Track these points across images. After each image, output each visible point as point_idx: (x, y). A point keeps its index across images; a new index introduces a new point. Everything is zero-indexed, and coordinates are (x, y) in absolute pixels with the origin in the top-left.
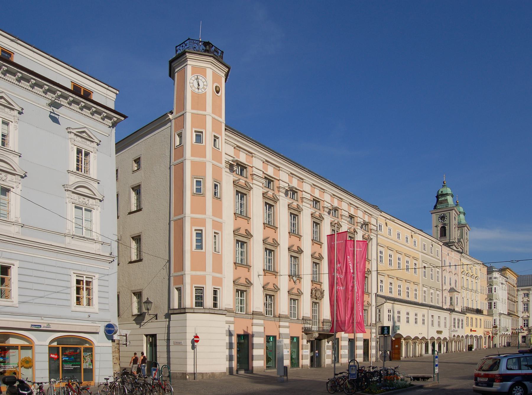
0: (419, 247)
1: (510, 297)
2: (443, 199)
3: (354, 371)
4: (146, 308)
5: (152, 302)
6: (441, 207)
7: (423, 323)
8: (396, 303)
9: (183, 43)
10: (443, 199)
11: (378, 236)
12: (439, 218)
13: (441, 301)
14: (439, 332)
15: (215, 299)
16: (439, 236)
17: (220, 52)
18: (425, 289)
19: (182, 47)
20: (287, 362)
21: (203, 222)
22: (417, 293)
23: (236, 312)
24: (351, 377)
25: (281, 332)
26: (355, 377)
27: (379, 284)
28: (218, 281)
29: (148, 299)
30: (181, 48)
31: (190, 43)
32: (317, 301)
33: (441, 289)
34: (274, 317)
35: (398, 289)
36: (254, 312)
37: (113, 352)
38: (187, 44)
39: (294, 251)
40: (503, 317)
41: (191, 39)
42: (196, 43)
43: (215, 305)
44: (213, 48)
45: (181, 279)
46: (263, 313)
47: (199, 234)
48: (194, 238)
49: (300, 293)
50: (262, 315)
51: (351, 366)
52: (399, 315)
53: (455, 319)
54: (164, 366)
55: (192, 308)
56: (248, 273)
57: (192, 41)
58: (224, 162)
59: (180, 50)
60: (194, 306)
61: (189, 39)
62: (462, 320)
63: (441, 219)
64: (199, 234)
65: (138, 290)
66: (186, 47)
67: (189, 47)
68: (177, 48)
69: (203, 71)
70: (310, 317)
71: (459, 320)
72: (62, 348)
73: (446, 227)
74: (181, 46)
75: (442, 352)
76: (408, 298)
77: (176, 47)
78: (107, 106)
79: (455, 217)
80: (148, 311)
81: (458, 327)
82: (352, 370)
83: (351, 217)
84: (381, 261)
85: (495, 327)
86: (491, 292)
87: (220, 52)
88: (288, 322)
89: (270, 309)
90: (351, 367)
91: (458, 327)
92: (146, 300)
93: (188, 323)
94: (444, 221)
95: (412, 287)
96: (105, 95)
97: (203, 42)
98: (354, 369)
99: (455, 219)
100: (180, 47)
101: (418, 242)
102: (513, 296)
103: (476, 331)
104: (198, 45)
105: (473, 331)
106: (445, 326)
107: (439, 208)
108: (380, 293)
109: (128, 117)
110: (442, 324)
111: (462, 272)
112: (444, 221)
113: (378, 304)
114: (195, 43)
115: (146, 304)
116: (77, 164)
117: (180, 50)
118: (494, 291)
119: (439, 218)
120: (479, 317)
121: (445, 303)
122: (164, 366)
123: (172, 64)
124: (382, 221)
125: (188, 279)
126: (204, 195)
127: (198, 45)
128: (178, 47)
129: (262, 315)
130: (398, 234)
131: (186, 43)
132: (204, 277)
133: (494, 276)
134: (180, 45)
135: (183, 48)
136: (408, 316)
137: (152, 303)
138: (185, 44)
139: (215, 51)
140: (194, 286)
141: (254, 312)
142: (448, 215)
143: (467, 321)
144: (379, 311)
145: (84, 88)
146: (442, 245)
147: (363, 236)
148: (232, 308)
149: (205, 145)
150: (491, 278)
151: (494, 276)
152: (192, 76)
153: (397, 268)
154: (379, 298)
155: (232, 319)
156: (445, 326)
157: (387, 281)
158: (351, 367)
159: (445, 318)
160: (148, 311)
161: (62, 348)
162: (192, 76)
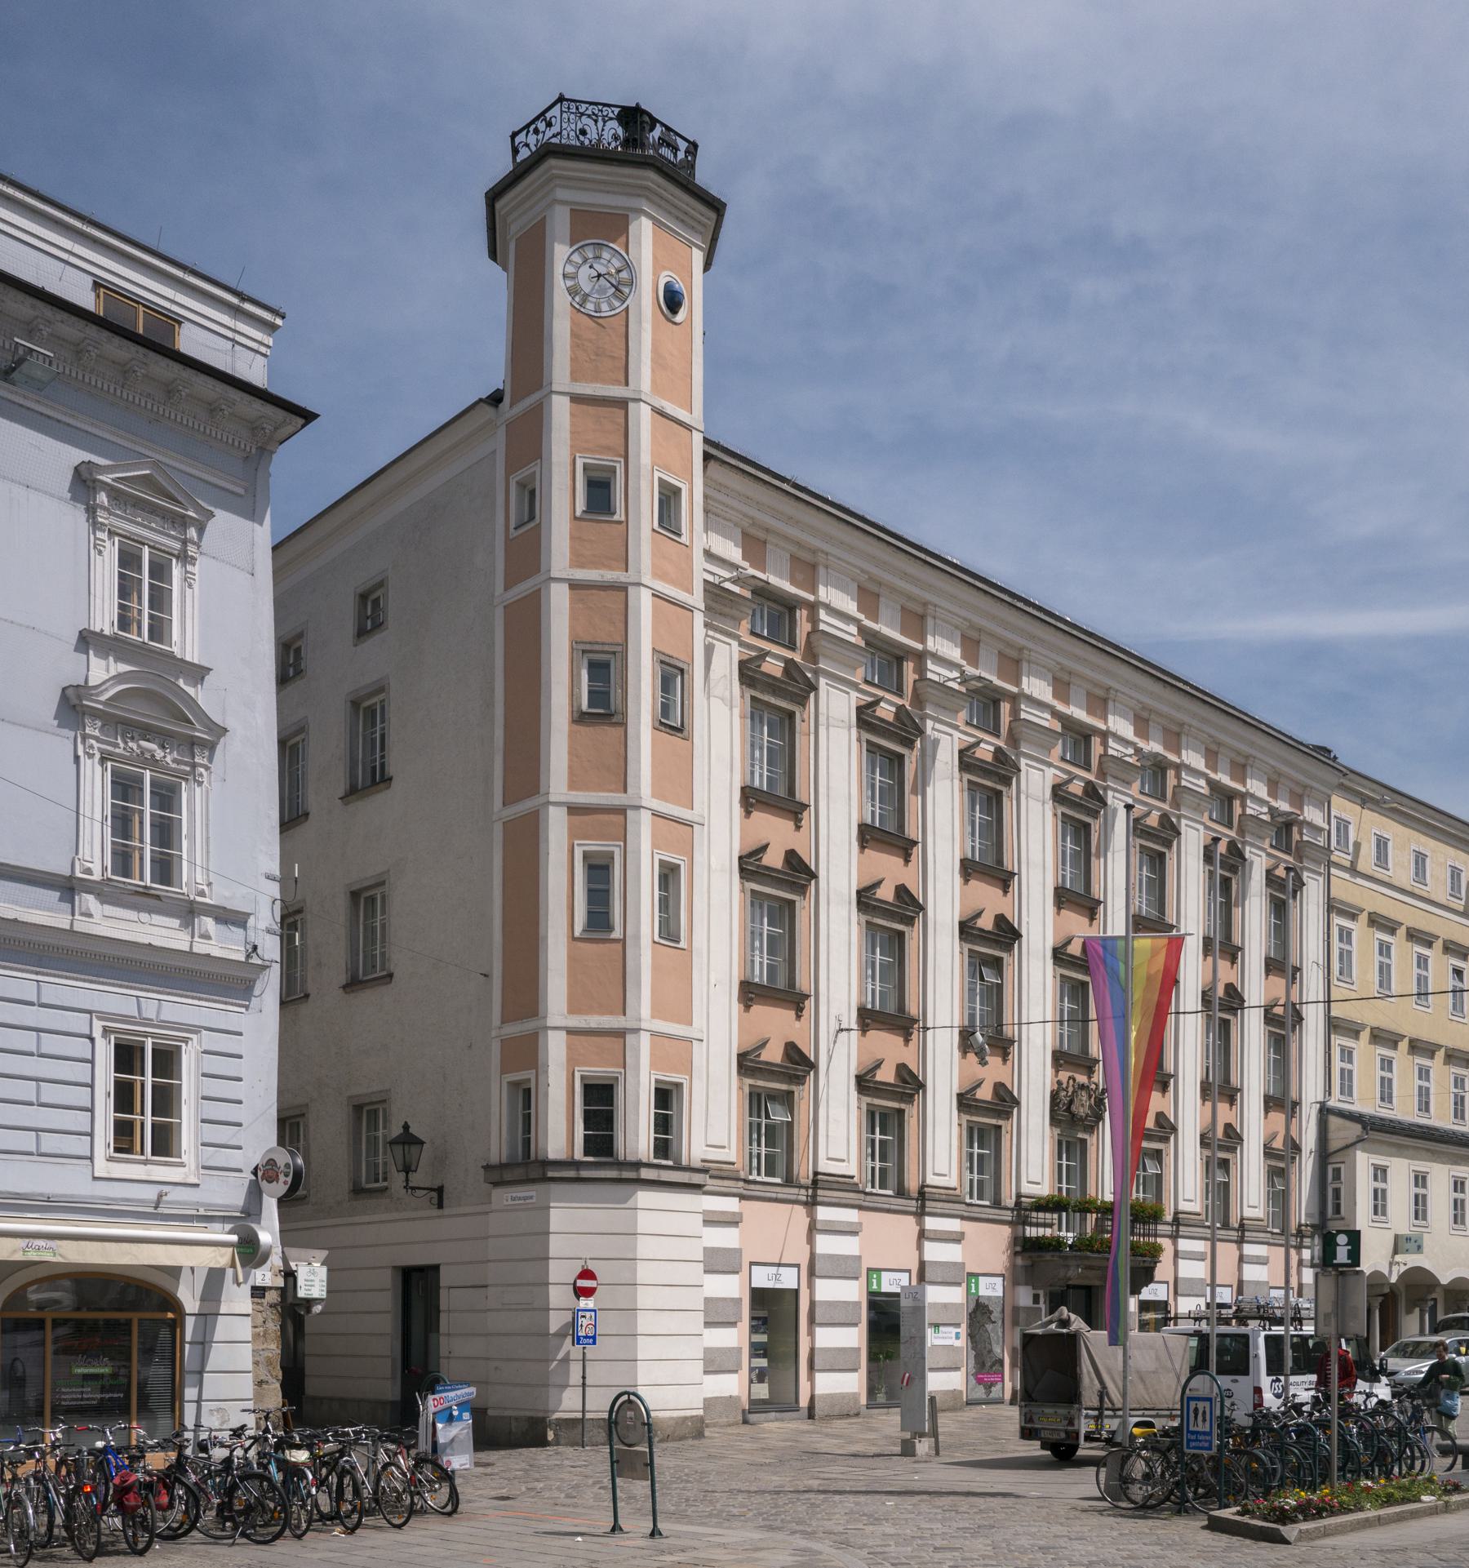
3: (1204, 1420)
4: (400, 1162)
5: (422, 1137)
9: (537, 118)
15: (663, 1124)
17: (683, 145)
19: (536, 131)
23: (751, 1178)
24: (1193, 1444)
25: (927, 1257)
26: (1206, 1445)
27: (1337, 1064)
28: (676, 1050)
29: (406, 1127)
30: (532, 139)
31: (565, 115)
35: (1419, 1083)
36: (820, 1177)
37: (256, 1336)
38: (553, 120)
41: (567, 100)
42: (589, 112)
43: (663, 1148)
44: (657, 132)
46: (856, 1180)
47: (599, 871)
49: (1005, 1102)
50: (855, 1189)
51: (1190, 1399)
54: (625, 1397)
57: (573, 105)
58: (699, 588)
59: (527, 145)
60: (579, 1154)
61: (561, 99)
64: (599, 871)
65: (373, 1093)
66: (549, 134)
67: (560, 133)
68: (517, 140)
70: (733, 1164)
72: (140, 1320)
74: (532, 128)
77: (514, 135)
78: (237, 375)
80: (407, 1173)
82: (1196, 1418)
87: (683, 145)
88: (734, 1195)
89: (755, 1152)
90: (1193, 1404)
92: (401, 1131)
96: (230, 334)
97: (617, 110)
98: (1204, 1412)
100: (528, 132)
104: (596, 121)
109: (318, 416)
114: (582, 114)
115: (398, 1149)
116: (121, 606)
117: (527, 145)
122: (625, 1397)
123: (498, 205)
125: (556, 1047)
127: (596, 121)
128: (521, 138)
131: (548, 115)
134: (528, 126)
135: (541, 136)
137: (422, 1143)
138: (545, 120)
139: (664, 141)
141: (820, 1177)
144: (1337, 1172)
145: (144, 306)
148: (733, 1159)
152: (575, 248)
153: (1374, 989)
154: (1334, 1121)
155: (731, 1205)
158: (1193, 1404)
160: (407, 1173)
161: (140, 1320)
162: (575, 248)
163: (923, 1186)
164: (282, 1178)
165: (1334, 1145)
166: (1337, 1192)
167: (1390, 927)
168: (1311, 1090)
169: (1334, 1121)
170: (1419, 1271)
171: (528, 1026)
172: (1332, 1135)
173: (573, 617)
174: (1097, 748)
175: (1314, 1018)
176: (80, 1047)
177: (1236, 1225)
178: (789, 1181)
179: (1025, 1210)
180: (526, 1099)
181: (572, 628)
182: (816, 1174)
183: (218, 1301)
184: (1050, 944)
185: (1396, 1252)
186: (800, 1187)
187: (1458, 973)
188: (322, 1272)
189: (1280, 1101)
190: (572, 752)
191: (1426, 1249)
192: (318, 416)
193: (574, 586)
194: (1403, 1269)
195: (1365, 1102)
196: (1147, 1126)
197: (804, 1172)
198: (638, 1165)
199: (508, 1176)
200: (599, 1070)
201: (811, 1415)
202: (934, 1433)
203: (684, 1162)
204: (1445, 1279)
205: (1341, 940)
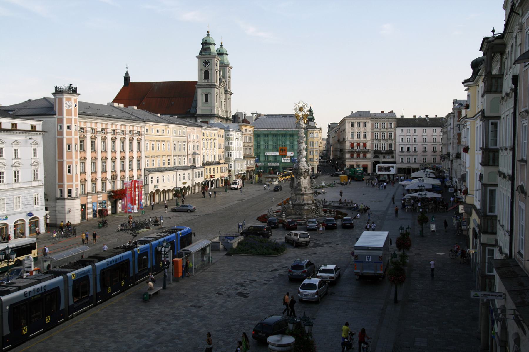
0: (171, 133)
2: (207, 46)
6: (205, 54)
10: (207, 46)
12: (204, 63)
13: (187, 162)
14: (185, 183)
16: (203, 78)
18: (175, 158)
20: (306, 281)
21: (71, 163)
22: (170, 161)
27: (146, 162)
34: (95, 193)
39: (104, 160)
40: (237, 162)
43: (61, 196)
45: (62, 186)
48: (68, 169)
50: (91, 193)
53: (196, 173)
55: (67, 198)
56: (85, 176)
63: (205, 64)
69: (70, 100)
73: (209, 71)
75: (188, 194)
79: (216, 63)
84: (147, 149)
85: (229, 171)
93: (66, 204)
94: (207, 66)
95: (166, 159)
99: (217, 64)
101: (171, 132)
106: (189, 178)
107: (203, 55)
109: (196, 56)
112: (207, 66)
113: (146, 174)
118: (230, 144)
119: (204, 63)
121: (190, 162)
125: (66, 186)
126: (71, 151)
129: (91, 193)
130: (158, 130)
132: (72, 185)
133: (230, 134)
140: (68, 189)
142: (210, 61)
144: (146, 178)
150: (228, 135)
151: (230, 134)
154: (146, 171)
156: (189, 178)
157: (150, 160)
166: (147, 181)
167: (159, 141)
168: (143, 167)
176: (12, 199)
179: (109, 192)
180: (62, 192)
184: (111, 158)
188: (431, 227)
192: (196, 56)
195: (150, 166)
196: (289, 161)
197: (86, 193)
198: (75, 198)
201: (87, 220)
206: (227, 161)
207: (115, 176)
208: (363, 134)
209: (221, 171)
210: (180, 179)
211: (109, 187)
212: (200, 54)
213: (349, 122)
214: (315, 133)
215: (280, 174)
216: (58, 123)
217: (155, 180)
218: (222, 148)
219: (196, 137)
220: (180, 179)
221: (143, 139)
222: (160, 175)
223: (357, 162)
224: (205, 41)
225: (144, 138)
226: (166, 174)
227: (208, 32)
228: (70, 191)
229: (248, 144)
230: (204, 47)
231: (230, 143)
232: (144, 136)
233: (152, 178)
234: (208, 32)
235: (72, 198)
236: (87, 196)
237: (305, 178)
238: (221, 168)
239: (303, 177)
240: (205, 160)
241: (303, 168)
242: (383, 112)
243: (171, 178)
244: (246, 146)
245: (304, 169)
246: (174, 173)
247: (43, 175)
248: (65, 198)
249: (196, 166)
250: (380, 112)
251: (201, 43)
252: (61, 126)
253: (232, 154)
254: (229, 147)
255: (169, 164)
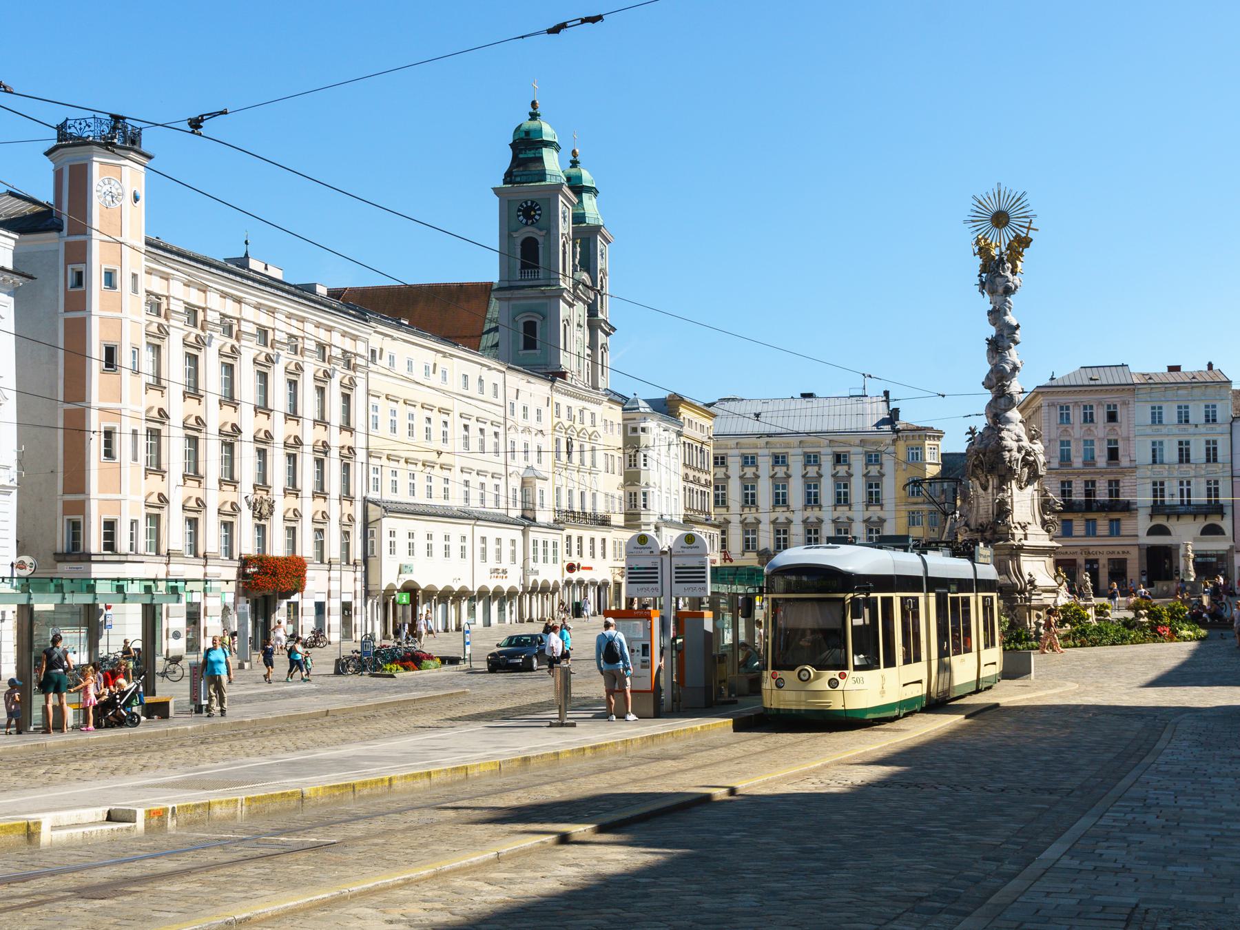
1: (691, 473)
2: (530, 154)
7: (463, 556)
8: (479, 523)
10: (530, 154)
11: (370, 374)
32: (263, 522)
33: (504, 473)
48: (103, 448)
52: (392, 539)
53: (535, 543)
62: (555, 544)
71: (545, 543)
72: (883, 598)
76: (429, 499)
81: (545, 560)
83: (322, 347)
86: (635, 465)
91: (545, 560)
95: (403, 471)
102: (700, 470)
103: (590, 568)
105: (584, 568)
106: (514, 559)
108: (373, 495)
109: (494, 189)
110: (506, 555)
111: (555, 427)
118: (642, 462)
119: (519, 210)
120: (599, 534)
124: (376, 341)
136: (447, 543)
143: (569, 545)
144: (372, 532)
146: (504, 370)
147: (184, 340)
149: (70, 267)
154: (371, 506)
156: (514, 559)
159: (513, 541)
163: (205, 553)
164: (28, 568)
165: (371, 518)
168: (358, 490)
169: (371, 506)
170: (410, 581)
171: (80, 497)
172: (370, 514)
173: (101, 331)
174: (270, 337)
175: (361, 455)
177: (165, 554)
178: (158, 554)
179: (245, 562)
180: (76, 530)
181: (100, 335)
182: (168, 550)
183: (919, 579)
185: (400, 573)
186: (163, 556)
187: (429, 419)
189: (347, 496)
190: (100, 385)
191: (414, 571)
193: (101, 317)
194: (404, 581)
199: (68, 558)
200: (110, 517)
202: (250, 661)
203: (119, 552)
204: (423, 586)
205: (373, 410)
206: (632, 519)
207: (266, 506)
208: (1105, 446)
209: (615, 556)
210: (484, 557)
211: (247, 545)
212: (505, 182)
213: (1053, 405)
214: (927, 447)
215: (915, 486)
216: (68, 262)
217: (402, 542)
218: (616, 471)
219: (532, 414)
220: (484, 557)
221: (361, 383)
222: (421, 527)
223: (1086, 550)
224: (523, 135)
225: (364, 381)
226: (439, 528)
227: (534, 104)
228: (110, 527)
229: (697, 474)
230: (521, 156)
231: (642, 458)
232: (364, 376)
233: (392, 534)
234: (534, 104)
235: (116, 554)
236: (167, 564)
237: (1021, 488)
238: (615, 543)
239: (1014, 482)
240: (564, 506)
241: (1014, 445)
242: (1174, 369)
243: (455, 545)
244: (691, 478)
245: (1020, 449)
246: (464, 529)
247: (15, 447)
248: (90, 555)
249: (534, 520)
250: (1166, 370)
251: (511, 142)
252: (79, 275)
253: (650, 498)
254: (639, 473)
255: (446, 497)
